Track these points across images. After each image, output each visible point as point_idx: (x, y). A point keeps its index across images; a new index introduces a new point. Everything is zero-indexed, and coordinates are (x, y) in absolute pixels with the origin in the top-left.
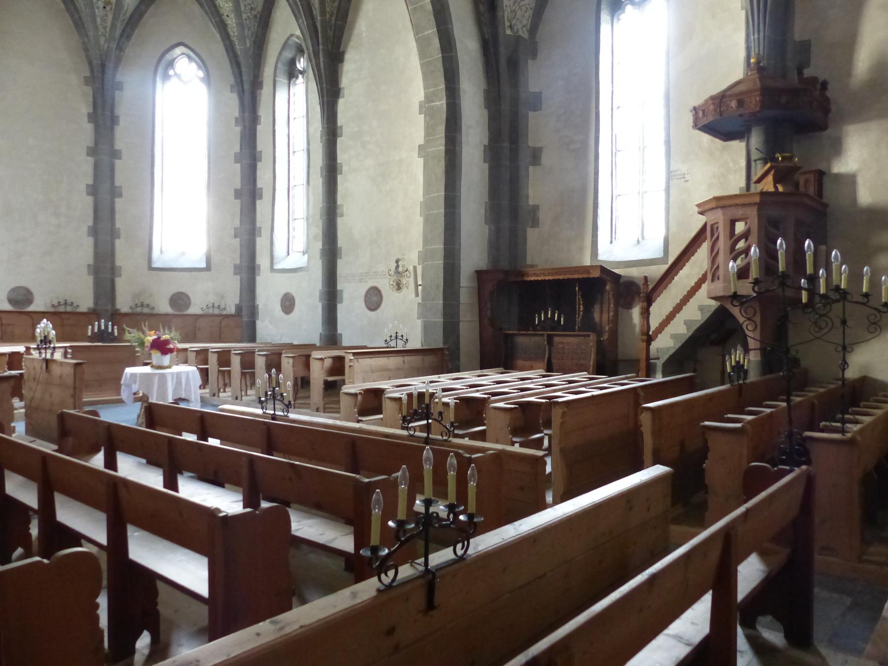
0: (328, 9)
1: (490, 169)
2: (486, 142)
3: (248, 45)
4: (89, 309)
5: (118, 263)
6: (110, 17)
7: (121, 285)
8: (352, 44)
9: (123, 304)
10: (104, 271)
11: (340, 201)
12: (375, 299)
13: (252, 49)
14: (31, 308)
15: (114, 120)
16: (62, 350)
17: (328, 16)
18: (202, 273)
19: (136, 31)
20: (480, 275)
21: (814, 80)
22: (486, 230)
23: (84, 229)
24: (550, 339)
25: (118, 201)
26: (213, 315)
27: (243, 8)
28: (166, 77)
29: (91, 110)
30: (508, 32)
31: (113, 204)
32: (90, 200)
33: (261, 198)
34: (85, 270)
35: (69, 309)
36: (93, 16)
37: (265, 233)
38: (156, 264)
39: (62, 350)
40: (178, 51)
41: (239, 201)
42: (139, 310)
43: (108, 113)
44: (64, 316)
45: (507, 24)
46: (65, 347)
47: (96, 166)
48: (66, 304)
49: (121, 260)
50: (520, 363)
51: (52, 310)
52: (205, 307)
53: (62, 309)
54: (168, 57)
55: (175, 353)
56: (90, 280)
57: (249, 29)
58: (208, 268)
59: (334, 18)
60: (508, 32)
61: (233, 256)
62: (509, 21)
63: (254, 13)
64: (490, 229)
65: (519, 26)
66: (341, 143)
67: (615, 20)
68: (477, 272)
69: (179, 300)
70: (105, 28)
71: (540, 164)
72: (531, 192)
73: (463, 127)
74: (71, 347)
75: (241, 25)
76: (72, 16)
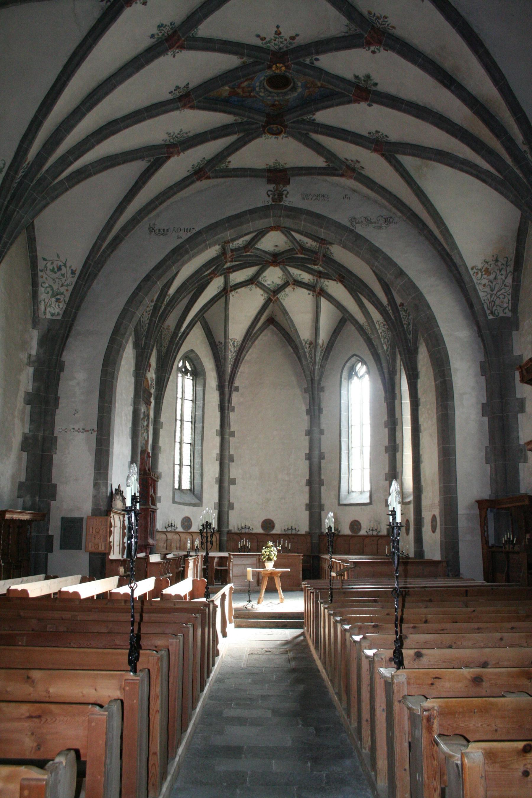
3: (385, 348)
5: (323, 502)
6: (313, 350)
14: (274, 532)
15: (320, 410)
17: (405, 326)
20: (481, 504)
23: (304, 482)
26: (373, 536)
27: (378, 327)
29: (308, 407)
30: (490, 317)
31: (320, 463)
32: (307, 462)
33: (398, 452)
34: (304, 507)
35: (294, 532)
36: (305, 353)
39: (257, 557)
40: (354, 359)
42: (371, 533)
44: (291, 537)
45: (488, 312)
47: (311, 442)
48: (292, 529)
51: (284, 533)
53: (290, 532)
57: (385, 338)
58: (340, 505)
59: (411, 326)
60: (490, 317)
65: (500, 310)
68: (477, 502)
69: (355, 525)
70: (311, 358)
71: (525, 412)
73: (456, 396)
76: (297, 355)
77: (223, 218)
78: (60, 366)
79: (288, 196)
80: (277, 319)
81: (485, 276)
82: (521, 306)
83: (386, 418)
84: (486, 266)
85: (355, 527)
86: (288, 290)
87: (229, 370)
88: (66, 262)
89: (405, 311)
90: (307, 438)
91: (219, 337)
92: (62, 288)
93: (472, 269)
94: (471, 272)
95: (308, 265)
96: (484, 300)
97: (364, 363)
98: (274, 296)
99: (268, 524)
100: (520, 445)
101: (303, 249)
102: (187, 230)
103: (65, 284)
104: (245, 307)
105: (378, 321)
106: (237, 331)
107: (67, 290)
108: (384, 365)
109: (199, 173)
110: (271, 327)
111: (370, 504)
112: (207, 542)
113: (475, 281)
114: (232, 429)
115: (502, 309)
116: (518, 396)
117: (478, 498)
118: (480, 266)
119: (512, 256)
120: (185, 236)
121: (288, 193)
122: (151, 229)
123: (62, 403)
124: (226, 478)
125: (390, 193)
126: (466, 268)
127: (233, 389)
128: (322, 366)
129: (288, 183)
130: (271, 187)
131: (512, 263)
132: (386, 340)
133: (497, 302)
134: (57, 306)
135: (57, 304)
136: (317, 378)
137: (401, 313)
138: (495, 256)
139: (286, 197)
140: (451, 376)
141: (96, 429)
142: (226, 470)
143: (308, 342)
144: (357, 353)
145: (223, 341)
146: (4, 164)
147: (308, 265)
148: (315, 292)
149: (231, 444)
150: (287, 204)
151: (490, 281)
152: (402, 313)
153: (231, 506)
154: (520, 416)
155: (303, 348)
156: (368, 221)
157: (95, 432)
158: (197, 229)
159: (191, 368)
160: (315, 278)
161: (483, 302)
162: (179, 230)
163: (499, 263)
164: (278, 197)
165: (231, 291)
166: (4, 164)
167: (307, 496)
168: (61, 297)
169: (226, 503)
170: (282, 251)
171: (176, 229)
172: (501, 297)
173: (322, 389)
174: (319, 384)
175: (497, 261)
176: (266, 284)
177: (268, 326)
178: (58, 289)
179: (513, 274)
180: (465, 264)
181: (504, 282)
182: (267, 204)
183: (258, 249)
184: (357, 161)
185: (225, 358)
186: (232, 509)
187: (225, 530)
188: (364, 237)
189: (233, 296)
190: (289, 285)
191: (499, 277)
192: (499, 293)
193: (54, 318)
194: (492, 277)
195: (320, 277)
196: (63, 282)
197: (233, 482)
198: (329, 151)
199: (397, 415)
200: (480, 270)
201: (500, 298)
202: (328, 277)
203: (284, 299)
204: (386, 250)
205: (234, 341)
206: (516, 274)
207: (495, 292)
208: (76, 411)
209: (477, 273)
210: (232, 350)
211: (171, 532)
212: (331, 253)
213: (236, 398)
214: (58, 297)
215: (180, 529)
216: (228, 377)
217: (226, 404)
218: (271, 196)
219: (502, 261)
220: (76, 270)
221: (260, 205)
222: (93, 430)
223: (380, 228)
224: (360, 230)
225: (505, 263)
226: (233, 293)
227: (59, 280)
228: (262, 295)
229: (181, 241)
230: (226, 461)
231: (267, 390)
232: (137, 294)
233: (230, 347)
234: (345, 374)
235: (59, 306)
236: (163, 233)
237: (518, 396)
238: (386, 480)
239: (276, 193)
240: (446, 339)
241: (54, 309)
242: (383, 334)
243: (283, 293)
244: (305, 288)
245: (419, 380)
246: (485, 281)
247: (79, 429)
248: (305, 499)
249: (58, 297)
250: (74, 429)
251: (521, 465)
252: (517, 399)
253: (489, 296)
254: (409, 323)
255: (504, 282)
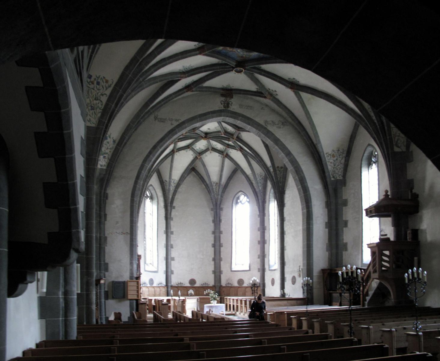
0: (279, 177)
1: (329, 230)
2: (327, 221)
3: (260, 188)
4: (213, 285)
5: (222, 269)
6: (218, 188)
7: (223, 276)
8: (287, 187)
9: (223, 283)
10: (217, 273)
11: (285, 245)
12: (294, 280)
13: (262, 190)
14: (196, 285)
15: (220, 221)
16: (197, 299)
17: (279, 179)
18: (248, 272)
19: (227, 190)
20: (323, 271)
21: (415, 194)
22: (327, 253)
23: (211, 259)
24: (341, 294)
25: (222, 248)
26: (229, 287)
27: (257, 177)
28: (237, 203)
29: (213, 219)
30: (333, 179)
31: (220, 249)
32: (213, 249)
33: (266, 243)
34: (211, 272)
35: (206, 285)
36: (213, 189)
37: (267, 256)
38: (233, 269)
40: (240, 193)
41: (259, 245)
42: (228, 285)
43: (218, 219)
45: (331, 176)
46: (198, 298)
47: (215, 238)
49: (223, 268)
50: (334, 303)
51: (201, 286)
52: (248, 284)
53: (204, 286)
54: (237, 196)
55: (137, 294)
56: (213, 275)
57: (260, 183)
58: (232, 271)
60: (333, 179)
61: (257, 265)
62: (332, 175)
63: (262, 177)
64: (329, 254)
65: (337, 175)
66: (286, 223)
67: (370, 170)
69: (241, 281)
70: (216, 192)
72: (345, 237)
74: (199, 298)
75: (257, 183)
76: (207, 189)
77: (196, 115)
78: (106, 197)
79: (232, 105)
80: (197, 169)
81: (332, 158)
82: (348, 174)
83: (259, 226)
84: (333, 153)
85: (241, 282)
86: (208, 153)
87: (171, 197)
88: (110, 135)
89: (279, 171)
90: (213, 235)
91: (166, 178)
92: (108, 150)
93: (326, 154)
94: (326, 156)
95: (223, 141)
96: (330, 170)
97: (245, 195)
98: (199, 156)
99: (192, 282)
100: (344, 243)
101: (226, 132)
102: (177, 120)
103: (109, 148)
104: (183, 160)
105: (258, 174)
106: (176, 175)
107: (110, 152)
108: (259, 198)
109: (188, 88)
110: (193, 173)
111: (249, 270)
112: (255, 292)
113: (327, 160)
114: (172, 230)
115: (338, 175)
116: (344, 219)
117: (322, 268)
118: (330, 153)
119: (346, 149)
120: (176, 124)
121: (232, 103)
122: (156, 118)
123: (108, 218)
124: (169, 257)
125: (289, 110)
126: (324, 153)
127: (173, 207)
128: (222, 196)
129: (232, 97)
130: (223, 99)
131: (345, 152)
132: (261, 184)
133: (337, 171)
134: (104, 161)
135: (104, 159)
136: (219, 203)
137: (277, 171)
138: (338, 148)
139: (231, 106)
140: (312, 208)
141: (129, 232)
142: (169, 253)
143: (215, 183)
144: (242, 190)
145: (168, 180)
146: (113, 82)
147: (223, 141)
148: (223, 155)
149: (172, 238)
150: (231, 110)
151: (334, 161)
152: (278, 172)
153: (172, 272)
154: (344, 229)
155: (212, 186)
156: (273, 123)
157: (129, 234)
158: (182, 120)
159: (150, 195)
160: (225, 147)
161: (330, 171)
162: (172, 120)
163: (340, 152)
164: (227, 105)
165: (177, 152)
166: (113, 82)
167: (213, 266)
168: (106, 156)
169: (169, 270)
170: (211, 131)
171: (170, 119)
172: (339, 169)
173: (221, 209)
174: (220, 206)
175: (339, 150)
176: (195, 149)
177: (191, 172)
178: (105, 151)
179: (346, 158)
180: (323, 152)
181: (340, 161)
182: (220, 109)
183: (200, 130)
184: (275, 91)
185: (169, 190)
186: (173, 274)
187: (169, 285)
188: (271, 132)
189: (176, 154)
190: (209, 150)
191: (339, 159)
192: (337, 167)
193: (102, 167)
194: (335, 159)
195: (228, 147)
196: (108, 146)
197: (173, 259)
198: (261, 84)
199: (266, 224)
200: (330, 155)
201: (338, 169)
202: (233, 147)
203: (204, 158)
204: (282, 140)
205: (174, 180)
206: (347, 158)
207: (335, 167)
208: (117, 223)
209: (328, 156)
210: (173, 185)
211: (161, 287)
212: (241, 136)
213: (174, 213)
214: (105, 155)
215: (149, 285)
216: (170, 200)
217: (169, 216)
218: (223, 104)
219: (341, 151)
220: (116, 140)
221: (217, 109)
222: (127, 233)
223: (280, 128)
224: (270, 128)
225: (342, 152)
226: (177, 153)
227: (106, 145)
228: (192, 155)
229: (173, 126)
230: (169, 248)
231: (193, 208)
232: (149, 156)
233: (172, 184)
234: (234, 201)
235: (105, 160)
236: (162, 120)
237: (344, 219)
238: (259, 258)
239: (226, 103)
240: (310, 189)
241: (102, 163)
242: (260, 181)
243: (204, 155)
244: (217, 152)
245: (285, 208)
246: (331, 161)
247: (119, 232)
248: (212, 268)
249: (105, 155)
250: (116, 232)
251: (344, 252)
252: (343, 220)
253: (333, 168)
254: (281, 177)
255: (340, 161)
